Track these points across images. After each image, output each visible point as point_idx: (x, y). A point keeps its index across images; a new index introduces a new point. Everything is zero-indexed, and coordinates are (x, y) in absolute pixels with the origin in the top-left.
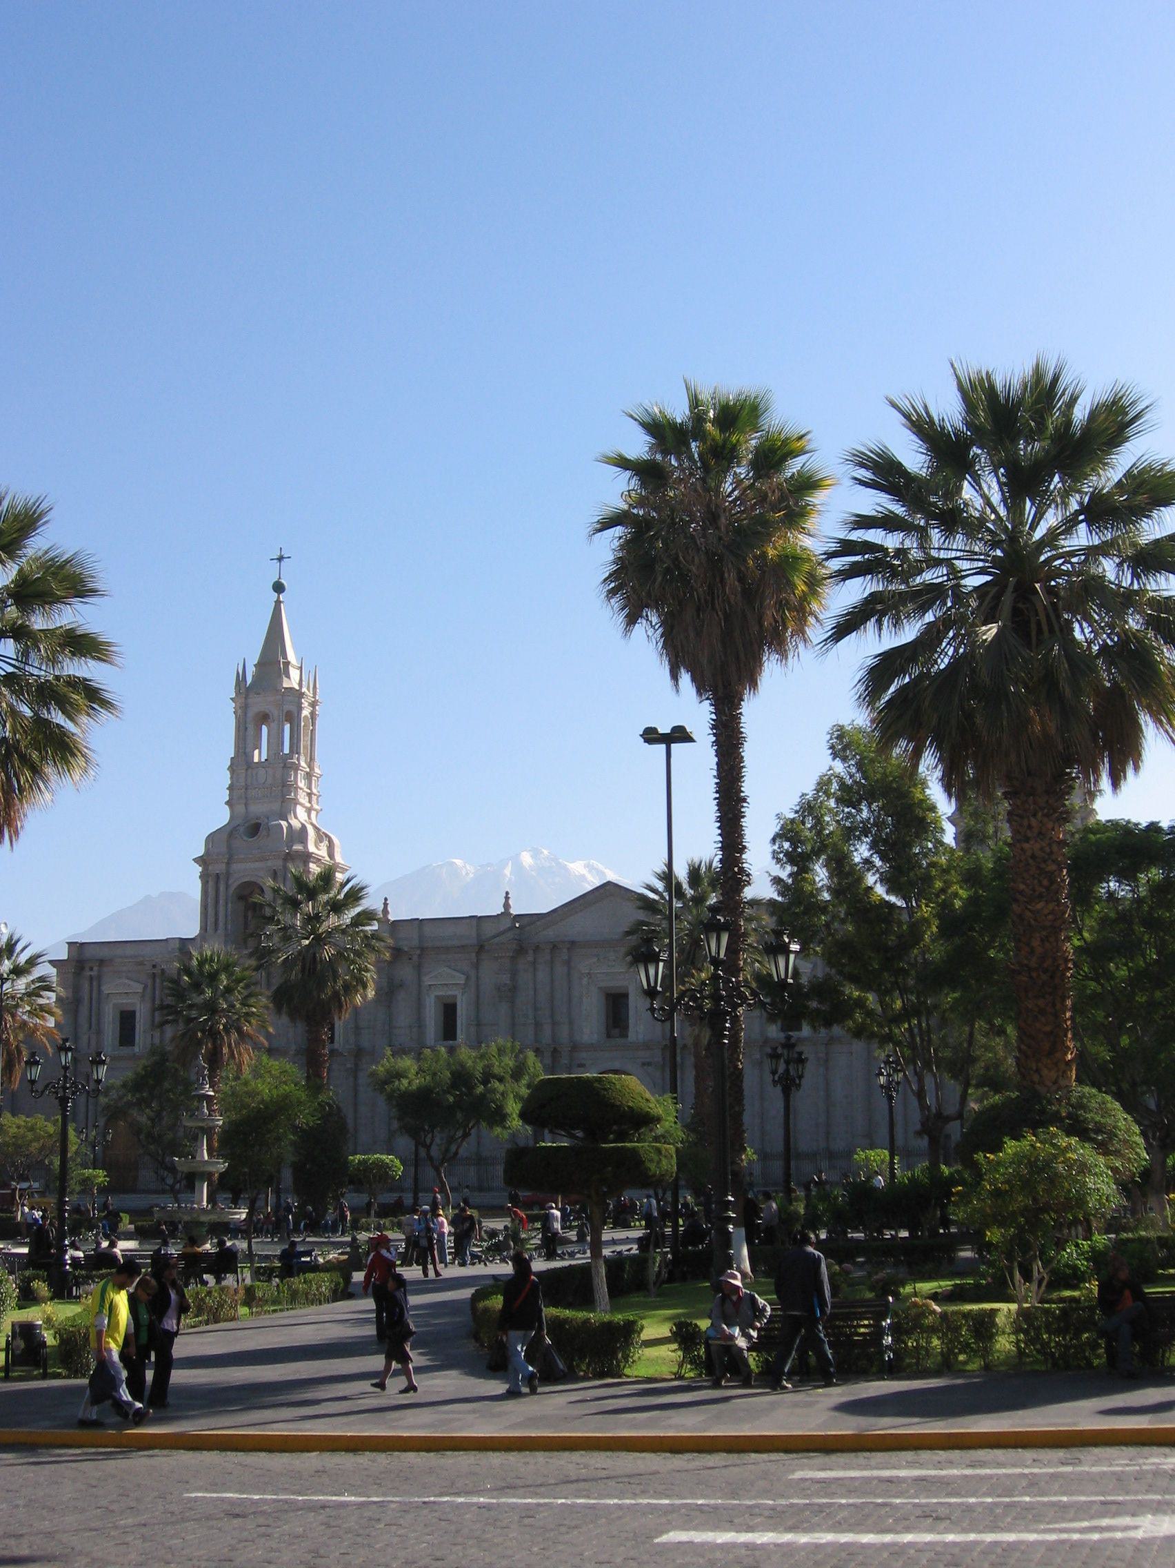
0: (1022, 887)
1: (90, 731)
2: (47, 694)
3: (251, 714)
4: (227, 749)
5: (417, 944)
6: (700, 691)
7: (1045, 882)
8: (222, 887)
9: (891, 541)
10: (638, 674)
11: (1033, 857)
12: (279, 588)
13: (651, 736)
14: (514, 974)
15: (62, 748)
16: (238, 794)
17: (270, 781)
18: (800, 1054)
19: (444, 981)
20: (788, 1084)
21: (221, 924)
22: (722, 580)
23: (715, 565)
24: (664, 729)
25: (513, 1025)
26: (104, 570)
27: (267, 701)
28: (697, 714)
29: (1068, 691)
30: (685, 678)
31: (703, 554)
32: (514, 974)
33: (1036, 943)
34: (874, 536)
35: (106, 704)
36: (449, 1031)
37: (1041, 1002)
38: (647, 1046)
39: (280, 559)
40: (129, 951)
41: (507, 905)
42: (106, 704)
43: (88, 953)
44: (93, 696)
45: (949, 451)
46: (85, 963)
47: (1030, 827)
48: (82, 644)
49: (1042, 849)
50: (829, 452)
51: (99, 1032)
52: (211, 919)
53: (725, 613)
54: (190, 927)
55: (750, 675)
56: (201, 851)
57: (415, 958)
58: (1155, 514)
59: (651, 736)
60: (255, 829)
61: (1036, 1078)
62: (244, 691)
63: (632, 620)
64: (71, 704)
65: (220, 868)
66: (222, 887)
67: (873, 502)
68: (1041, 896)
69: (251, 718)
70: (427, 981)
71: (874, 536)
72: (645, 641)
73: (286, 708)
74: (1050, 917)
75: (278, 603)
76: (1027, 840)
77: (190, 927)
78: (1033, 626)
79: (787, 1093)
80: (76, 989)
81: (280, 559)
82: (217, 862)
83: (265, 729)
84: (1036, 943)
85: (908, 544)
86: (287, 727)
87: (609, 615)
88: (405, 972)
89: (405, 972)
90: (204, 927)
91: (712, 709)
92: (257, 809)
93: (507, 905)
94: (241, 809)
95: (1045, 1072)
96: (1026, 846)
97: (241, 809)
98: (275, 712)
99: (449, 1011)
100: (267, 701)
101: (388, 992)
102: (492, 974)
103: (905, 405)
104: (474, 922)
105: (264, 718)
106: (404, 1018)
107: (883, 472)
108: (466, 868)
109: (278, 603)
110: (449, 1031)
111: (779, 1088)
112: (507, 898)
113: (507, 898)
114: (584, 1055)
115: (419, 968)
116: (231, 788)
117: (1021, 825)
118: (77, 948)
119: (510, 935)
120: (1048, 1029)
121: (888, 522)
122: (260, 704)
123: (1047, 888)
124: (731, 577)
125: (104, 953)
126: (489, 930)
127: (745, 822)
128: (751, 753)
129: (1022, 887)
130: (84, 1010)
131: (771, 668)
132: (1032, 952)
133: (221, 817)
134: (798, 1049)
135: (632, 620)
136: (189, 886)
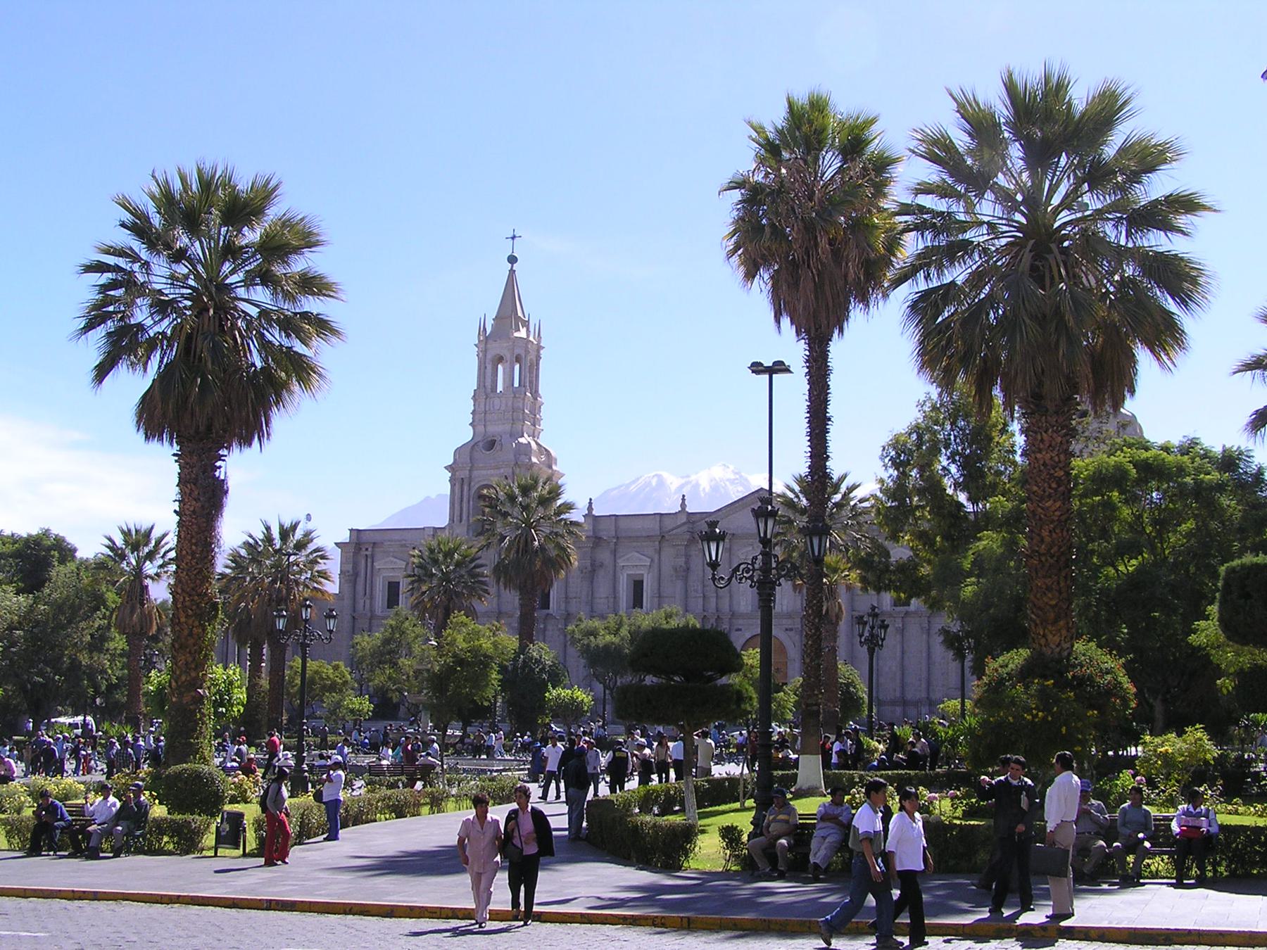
0: (1035, 488)
1: (319, 351)
2: (289, 325)
3: (489, 357)
4: (471, 382)
5: (610, 533)
6: (798, 333)
7: (1054, 485)
8: (466, 488)
9: (941, 205)
10: (752, 320)
11: (1044, 464)
12: (512, 260)
13: (757, 368)
14: (688, 557)
15: (302, 370)
16: (479, 417)
17: (503, 408)
18: (883, 621)
19: (634, 563)
20: (873, 643)
21: (464, 518)
22: (816, 245)
23: (809, 228)
24: (768, 363)
25: (686, 597)
26: (325, 226)
27: (508, 353)
28: (794, 350)
29: (1071, 323)
30: (786, 321)
31: (808, 228)
32: (688, 557)
33: (1045, 533)
34: (927, 201)
35: (334, 332)
36: (637, 601)
37: (1048, 581)
38: (789, 616)
39: (513, 238)
40: (397, 536)
41: (683, 505)
42: (334, 332)
43: (364, 538)
44: (323, 326)
45: (980, 124)
46: (362, 546)
47: (1042, 441)
48: (312, 284)
49: (1052, 458)
50: (894, 134)
51: (372, 598)
52: (457, 513)
53: (818, 270)
54: (442, 520)
55: (839, 319)
56: (450, 461)
57: (612, 545)
58: (1145, 178)
59: (757, 368)
60: (491, 445)
61: (1043, 641)
62: (485, 341)
63: (750, 275)
64: (304, 332)
65: (464, 474)
66: (466, 488)
67: (930, 173)
68: (1050, 496)
69: (488, 363)
70: (621, 563)
71: (927, 201)
72: (759, 294)
73: (517, 351)
74: (1057, 513)
75: (512, 272)
76: (1040, 451)
77: (442, 520)
78: (1047, 275)
79: (871, 652)
80: (355, 565)
81: (513, 238)
82: (463, 469)
83: (500, 367)
84: (1045, 533)
85: (954, 208)
86: (517, 367)
87: (732, 271)
88: (604, 556)
89: (604, 556)
90: (452, 520)
91: (806, 347)
92: (494, 429)
93: (683, 505)
94: (481, 429)
95: (1050, 637)
96: (1039, 456)
97: (481, 429)
98: (507, 355)
99: (638, 586)
100: (508, 353)
101: (592, 571)
102: (671, 558)
103: (957, 92)
104: (658, 518)
105: (500, 359)
106: (603, 590)
107: (938, 149)
108: (673, 482)
109: (512, 272)
110: (637, 601)
111: (865, 647)
112: (683, 499)
113: (683, 499)
114: (741, 621)
115: (614, 553)
116: (473, 413)
117: (1035, 439)
118: (357, 535)
119: (685, 528)
120: (1053, 602)
121: (942, 191)
122: (496, 349)
123: (1055, 490)
124: (823, 243)
125: (378, 538)
126: (669, 524)
127: (830, 437)
128: (834, 381)
129: (1035, 488)
130: (361, 580)
131: (856, 315)
132: (1042, 541)
133: (467, 435)
134: (880, 618)
135: (750, 275)
136: (442, 486)
